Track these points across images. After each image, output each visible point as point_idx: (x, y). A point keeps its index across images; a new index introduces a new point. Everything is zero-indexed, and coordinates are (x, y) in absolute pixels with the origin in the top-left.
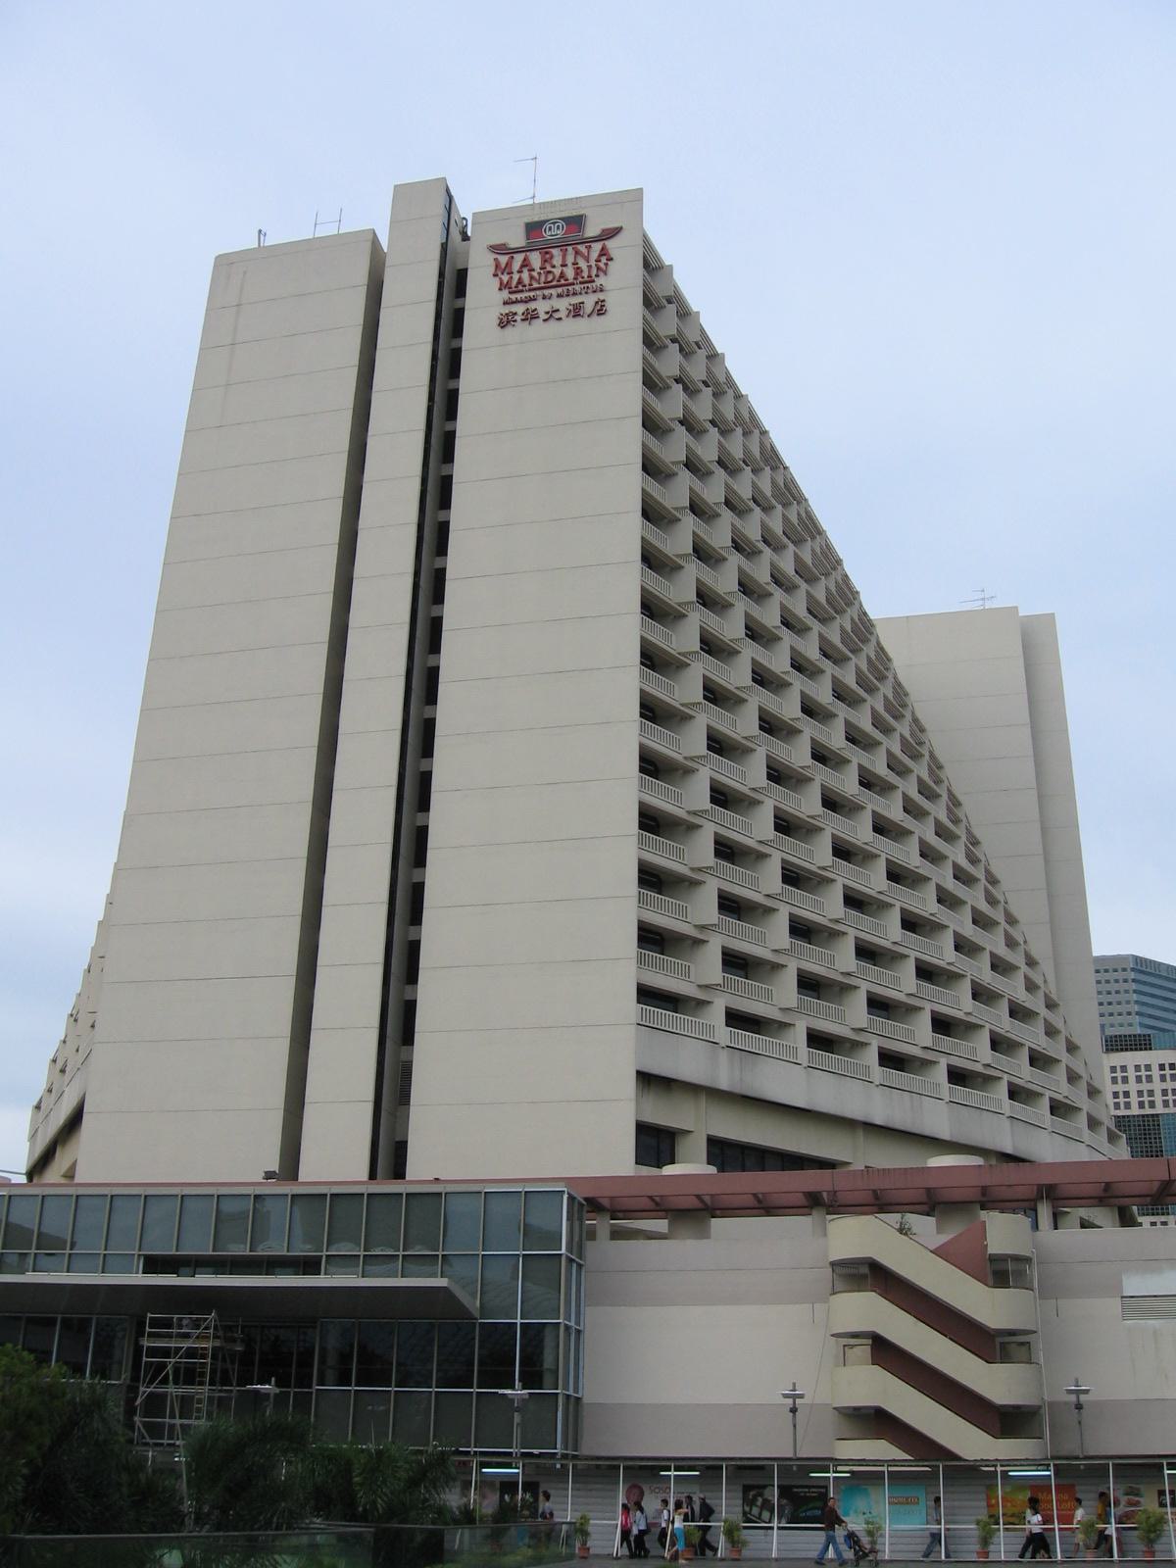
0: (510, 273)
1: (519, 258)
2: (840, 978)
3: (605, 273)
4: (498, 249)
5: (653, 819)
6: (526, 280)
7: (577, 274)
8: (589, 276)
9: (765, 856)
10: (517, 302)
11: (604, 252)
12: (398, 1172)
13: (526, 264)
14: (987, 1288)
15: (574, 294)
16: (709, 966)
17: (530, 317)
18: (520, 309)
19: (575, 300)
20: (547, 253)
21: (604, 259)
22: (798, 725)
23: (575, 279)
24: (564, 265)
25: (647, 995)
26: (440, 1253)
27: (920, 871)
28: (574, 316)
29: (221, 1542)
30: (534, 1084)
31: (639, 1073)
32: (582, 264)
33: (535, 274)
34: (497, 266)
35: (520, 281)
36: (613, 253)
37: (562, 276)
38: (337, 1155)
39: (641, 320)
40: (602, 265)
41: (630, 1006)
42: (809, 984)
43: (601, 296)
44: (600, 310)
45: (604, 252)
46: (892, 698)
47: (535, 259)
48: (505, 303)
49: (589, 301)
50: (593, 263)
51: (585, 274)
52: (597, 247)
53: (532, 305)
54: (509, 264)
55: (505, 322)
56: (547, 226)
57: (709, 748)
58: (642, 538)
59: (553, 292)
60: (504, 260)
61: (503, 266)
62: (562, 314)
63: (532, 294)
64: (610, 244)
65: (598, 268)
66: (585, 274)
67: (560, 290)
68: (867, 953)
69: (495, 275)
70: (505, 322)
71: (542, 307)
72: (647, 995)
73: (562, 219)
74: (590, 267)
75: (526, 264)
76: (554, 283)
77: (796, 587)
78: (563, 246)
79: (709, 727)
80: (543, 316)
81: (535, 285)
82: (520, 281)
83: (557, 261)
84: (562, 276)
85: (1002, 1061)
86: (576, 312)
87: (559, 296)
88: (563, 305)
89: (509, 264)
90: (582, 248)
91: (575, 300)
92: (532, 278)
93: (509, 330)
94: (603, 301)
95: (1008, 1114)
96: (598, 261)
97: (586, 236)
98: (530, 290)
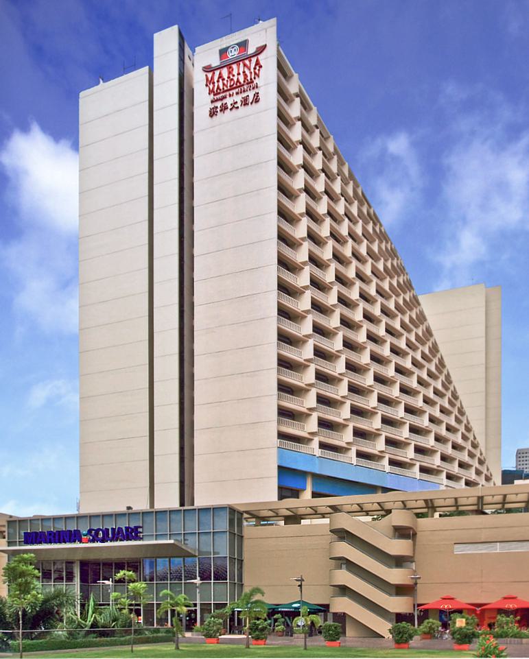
0: (214, 83)
1: (217, 73)
2: (375, 431)
3: (258, 76)
4: (208, 69)
5: (450, 428)
6: (221, 87)
7: (245, 78)
8: (251, 79)
9: (341, 380)
10: (217, 100)
11: (258, 63)
12: (153, 507)
13: (220, 76)
14: (346, 557)
15: (244, 91)
16: (348, 436)
17: (224, 108)
18: (219, 104)
19: (244, 95)
20: (230, 68)
21: (258, 68)
22: (385, 338)
23: (244, 81)
24: (239, 74)
25: (282, 436)
26: (197, 531)
27: (417, 389)
28: (244, 105)
29: (151, 620)
30: (239, 470)
31: (280, 468)
32: (247, 72)
33: (225, 82)
34: (207, 79)
35: (218, 88)
36: (262, 63)
37: (238, 81)
38: (168, 499)
39: (276, 102)
40: (257, 71)
41: (275, 441)
42: (390, 442)
43: (256, 90)
44: (256, 100)
45: (258, 63)
46: (402, 304)
47: (225, 72)
48: (212, 102)
49: (251, 94)
50: (252, 70)
51: (249, 78)
52: (254, 60)
53: (224, 101)
54: (212, 78)
55: (213, 113)
56: (230, 50)
57: (314, 331)
58: (309, 250)
59: (235, 91)
60: (210, 75)
61: (210, 79)
62: (239, 104)
63: (224, 94)
64: (261, 57)
65: (255, 73)
66: (249, 78)
67: (237, 90)
68: (414, 430)
69: (207, 85)
70: (213, 113)
71: (229, 101)
72: (282, 436)
73: (237, 44)
74: (251, 73)
75: (220, 76)
76: (235, 86)
77: (366, 261)
78: (237, 63)
79: (314, 321)
80: (230, 107)
81: (225, 88)
82: (218, 88)
83: (235, 72)
84: (238, 81)
85: (445, 465)
86: (245, 102)
87: (237, 93)
88: (238, 99)
89: (212, 78)
90: (247, 62)
91: (244, 95)
92: (224, 84)
93: (214, 117)
94: (258, 93)
95: (418, 478)
96: (255, 68)
97: (249, 53)
98: (223, 92)
